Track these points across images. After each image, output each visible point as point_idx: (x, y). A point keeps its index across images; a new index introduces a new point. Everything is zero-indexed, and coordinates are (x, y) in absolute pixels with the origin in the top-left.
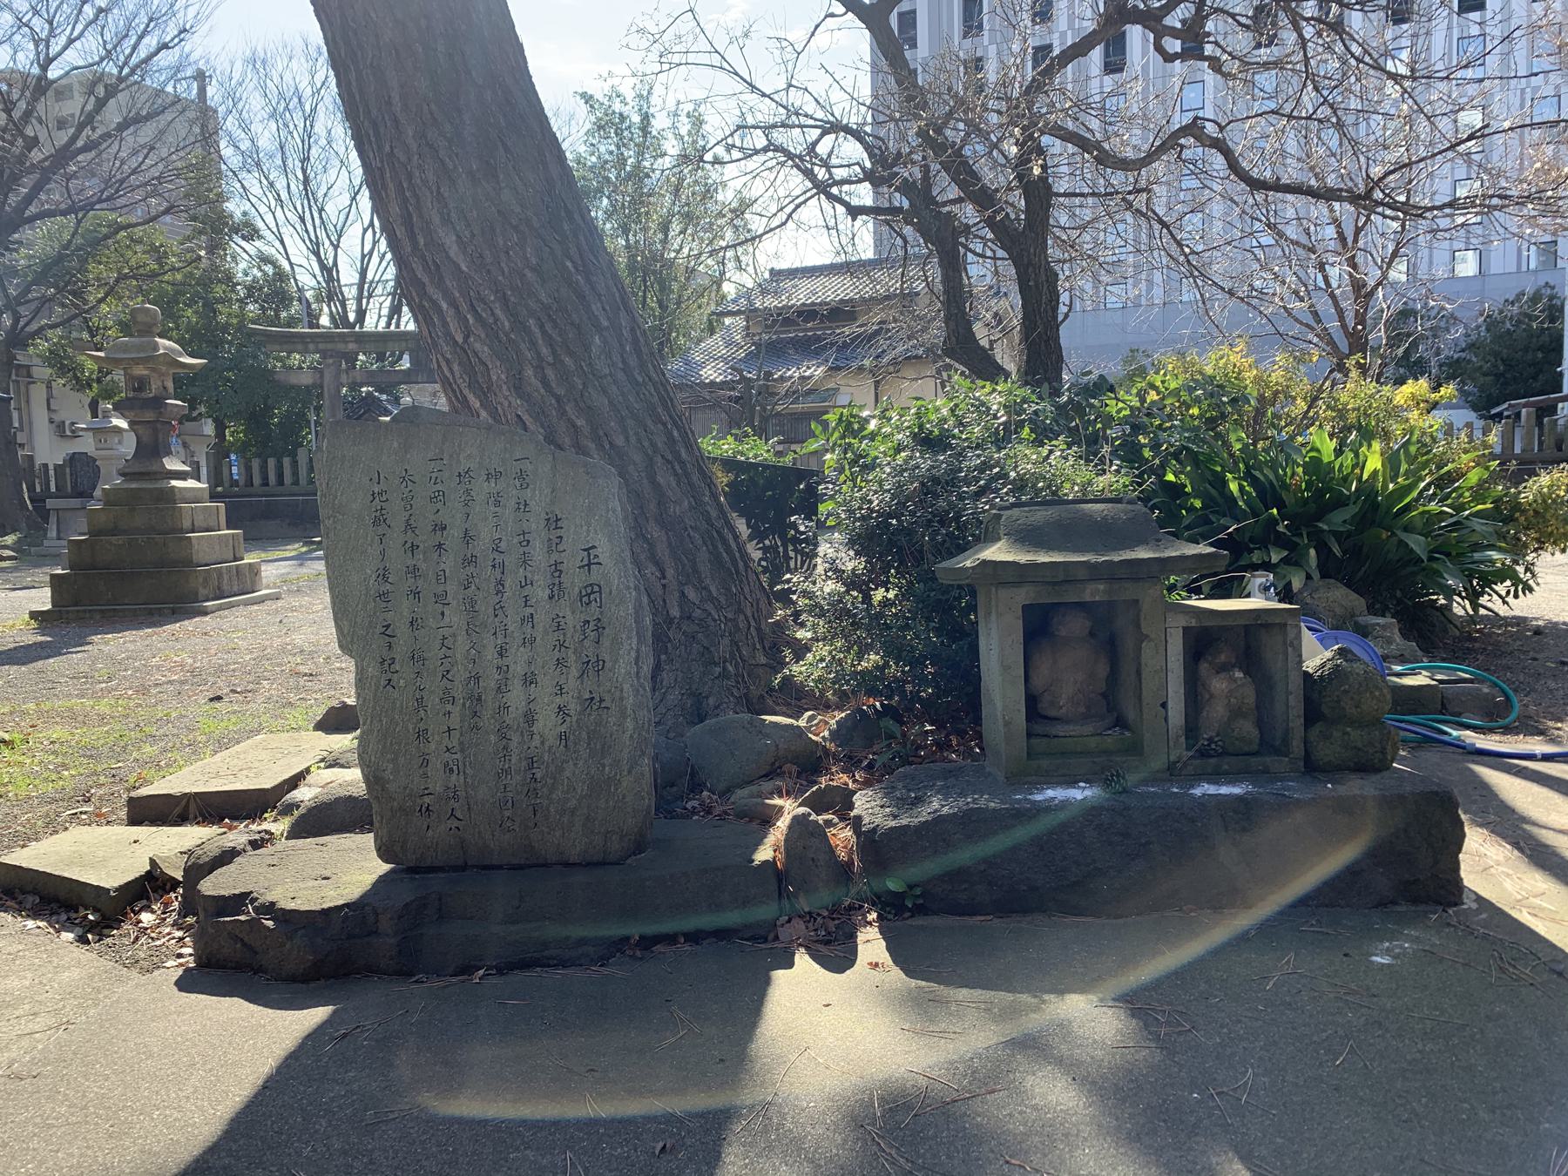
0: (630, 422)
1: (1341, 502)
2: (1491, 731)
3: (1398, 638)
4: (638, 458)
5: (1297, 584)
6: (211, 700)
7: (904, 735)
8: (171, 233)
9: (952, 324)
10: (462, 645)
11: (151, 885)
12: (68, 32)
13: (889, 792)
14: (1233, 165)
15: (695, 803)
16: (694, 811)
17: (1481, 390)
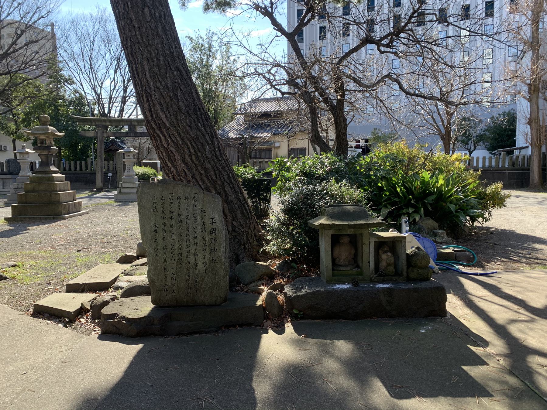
0: (217, 172)
1: (431, 194)
2: (469, 266)
3: (446, 237)
4: (219, 182)
5: (417, 219)
6: (78, 251)
7: (298, 268)
8: (43, 83)
9: (314, 132)
10: (177, 245)
11: (82, 311)
12: (7, 11)
13: (294, 285)
14: (401, 88)
15: (239, 288)
16: (238, 290)
17: (491, 144)
